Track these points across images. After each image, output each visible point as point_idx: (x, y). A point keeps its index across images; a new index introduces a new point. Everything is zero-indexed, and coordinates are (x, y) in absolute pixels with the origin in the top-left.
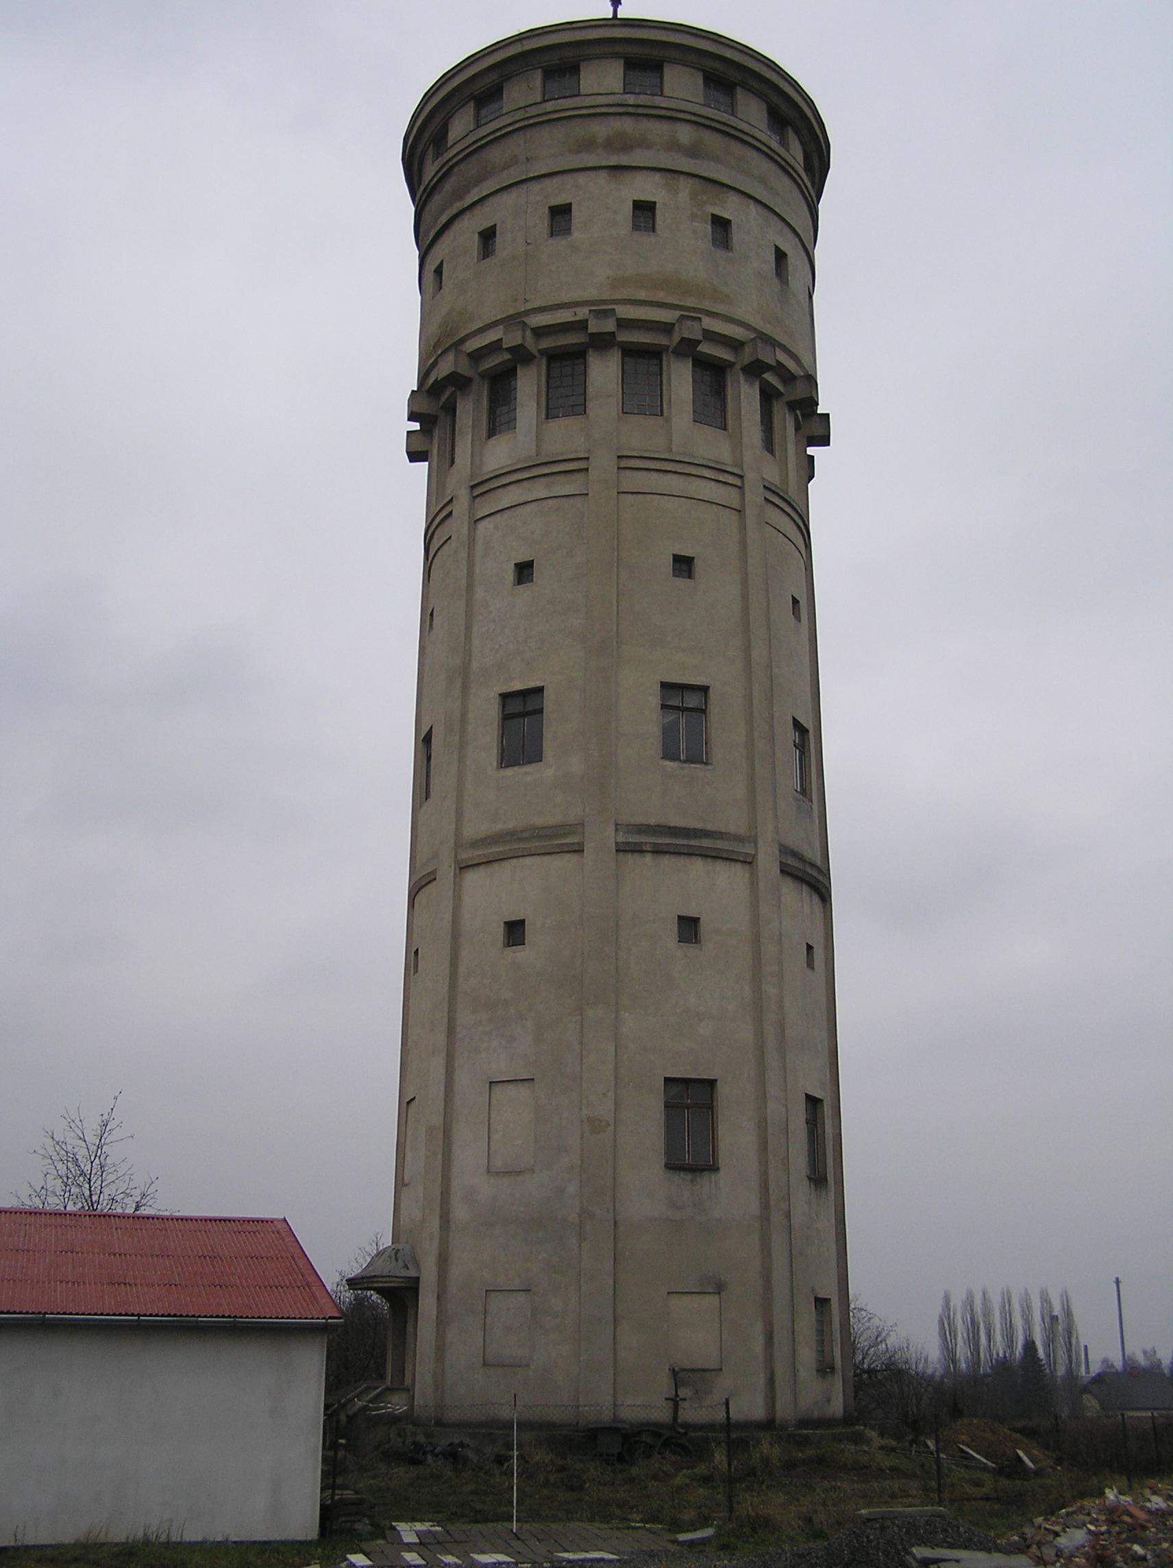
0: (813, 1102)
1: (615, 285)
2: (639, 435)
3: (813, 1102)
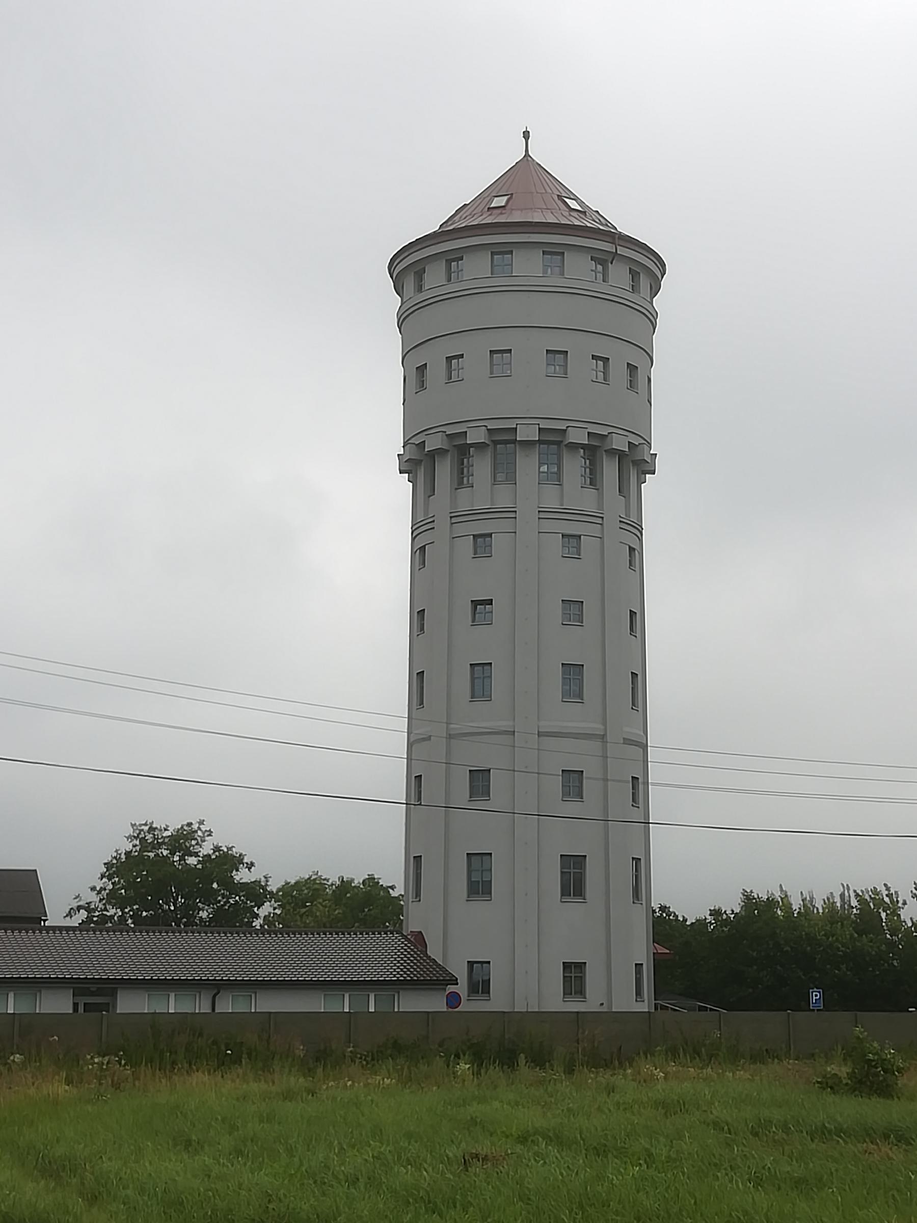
0: (632, 614)
1: (526, 352)
2: (550, 498)
3: (632, 614)
